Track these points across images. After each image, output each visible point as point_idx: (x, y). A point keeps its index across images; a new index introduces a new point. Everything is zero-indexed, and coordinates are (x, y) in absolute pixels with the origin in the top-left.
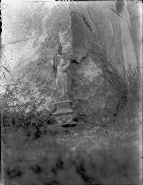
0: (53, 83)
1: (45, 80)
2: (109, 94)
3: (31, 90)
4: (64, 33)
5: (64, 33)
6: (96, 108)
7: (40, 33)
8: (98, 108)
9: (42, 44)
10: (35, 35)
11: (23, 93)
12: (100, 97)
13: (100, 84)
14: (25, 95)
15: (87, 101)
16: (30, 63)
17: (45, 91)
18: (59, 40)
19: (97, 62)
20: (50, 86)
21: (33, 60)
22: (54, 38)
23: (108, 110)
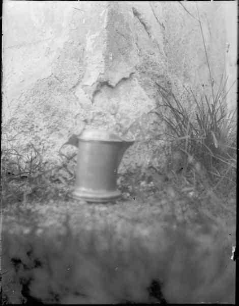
0: (69, 116)
1: (58, 111)
2: (160, 144)
3: (35, 125)
4: (93, 36)
5: (93, 36)
11: (23, 129)
12: (144, 147)
13: (148, 125)
16: (38, 80)
17: (56, 128)
18: (86, 46)
19: (147, 88)
20: (63, 120)
23: (155, 169)
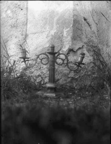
3: (42, 67)
4: (67, 30)
5: (67, 30)
6: (83, 85)
7: (52, 28)
8: (84, 84)
9: (52, 36)
10: (48, 29)
11: (36, 68)
14: (38, 70)
15: (77, 79)
16: (43, 48)
18: (63, 34)
21: (45, 47)
22: (60, 32)
